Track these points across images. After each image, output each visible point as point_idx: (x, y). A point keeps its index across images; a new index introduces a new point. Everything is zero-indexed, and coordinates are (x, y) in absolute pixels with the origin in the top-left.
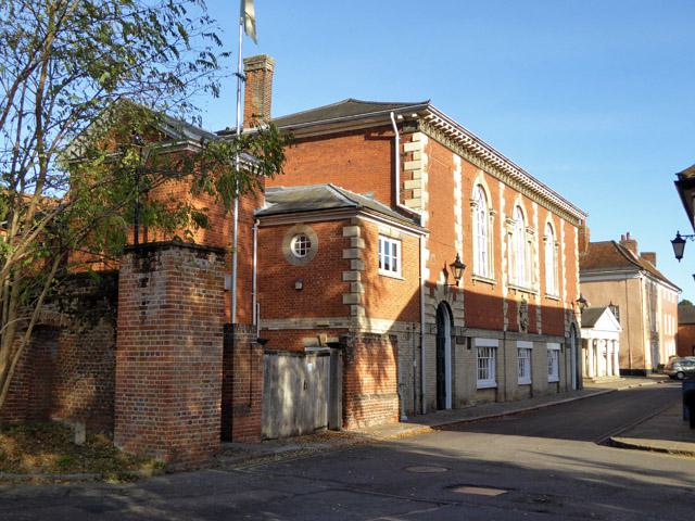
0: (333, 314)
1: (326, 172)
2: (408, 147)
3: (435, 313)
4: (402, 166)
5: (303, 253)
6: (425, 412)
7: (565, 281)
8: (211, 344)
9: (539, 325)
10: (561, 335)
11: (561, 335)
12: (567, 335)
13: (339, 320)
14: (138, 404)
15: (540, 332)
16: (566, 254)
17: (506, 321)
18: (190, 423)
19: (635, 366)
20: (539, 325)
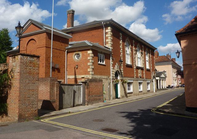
0: (86, 74)
1: (87, 38)
2: (107, 31)
3: (115, 73)
4: (105, 36)
5: (78, 58)
6: (119, 96)
7: (151, 65)
8: (34, 83)
9: (144, 76)
10: (151, 79)
11: (151, 79)
12: (152, 79)
13: (87, 76)
14: (12, 101)
15: (135, 77)
16: (152, 64)
17: (135, 75)
18: (27, 107)
19: (59, 44)
20: (144, 76)
